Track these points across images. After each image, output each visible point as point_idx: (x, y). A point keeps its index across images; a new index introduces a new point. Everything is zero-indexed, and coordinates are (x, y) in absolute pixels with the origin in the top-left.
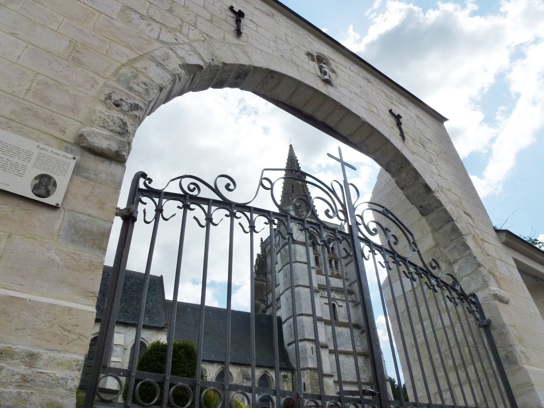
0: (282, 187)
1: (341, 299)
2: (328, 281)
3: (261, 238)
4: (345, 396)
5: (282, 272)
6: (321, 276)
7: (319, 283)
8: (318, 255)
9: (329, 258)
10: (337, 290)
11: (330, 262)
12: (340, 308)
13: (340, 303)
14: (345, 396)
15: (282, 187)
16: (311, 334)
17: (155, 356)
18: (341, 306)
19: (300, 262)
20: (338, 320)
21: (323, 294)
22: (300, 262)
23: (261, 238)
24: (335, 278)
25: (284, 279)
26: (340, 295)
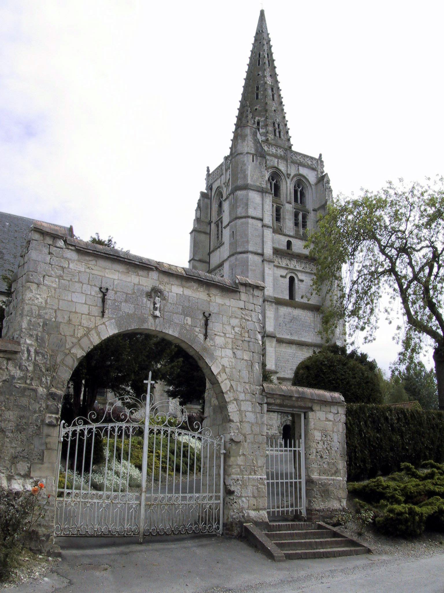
0: (246, 72)
1: (303, 270)
2: (289, 244)
3: (208, 168)
4: (150, 373)
5: (228, 228)
6: (281, 236)
7: (277, 246)
8: (280, 204)
9: (294, 210)
10: (299, 257)
11: (296, 215)
12: (300, 283)
13: (301, 276)
14: (150, 373)
15: (246, 72)
16: (8, 399)
17: (166, 426)
18: (302, 281)
19: (253, 218)
20: (295, 300)
21: (281, 263)
22: (253, 218)
23: (208, 168)
24: (300, 240)
25: (230, 240)
26: (303, 265)
